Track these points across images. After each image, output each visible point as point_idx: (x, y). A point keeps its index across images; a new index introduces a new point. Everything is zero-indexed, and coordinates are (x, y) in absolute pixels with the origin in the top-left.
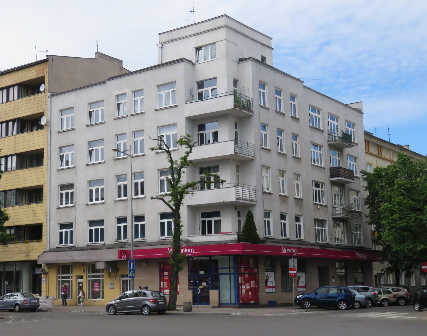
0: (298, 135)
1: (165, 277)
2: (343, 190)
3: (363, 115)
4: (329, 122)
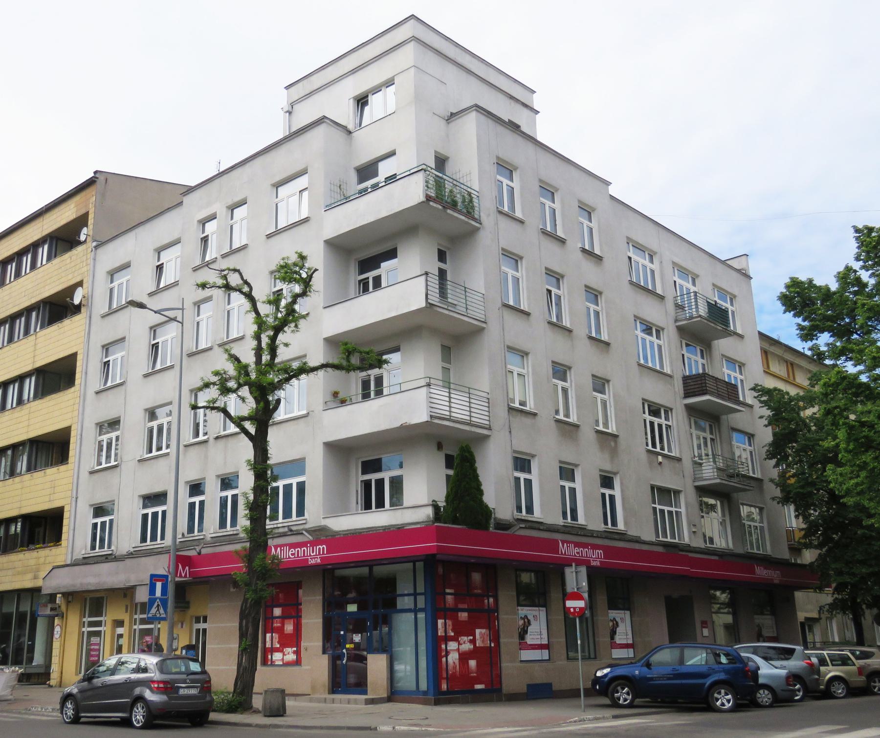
0: (601, 293)
1: (275, 621)
2: (717, 431)
3: (752, 280)
4: (675, 282)
